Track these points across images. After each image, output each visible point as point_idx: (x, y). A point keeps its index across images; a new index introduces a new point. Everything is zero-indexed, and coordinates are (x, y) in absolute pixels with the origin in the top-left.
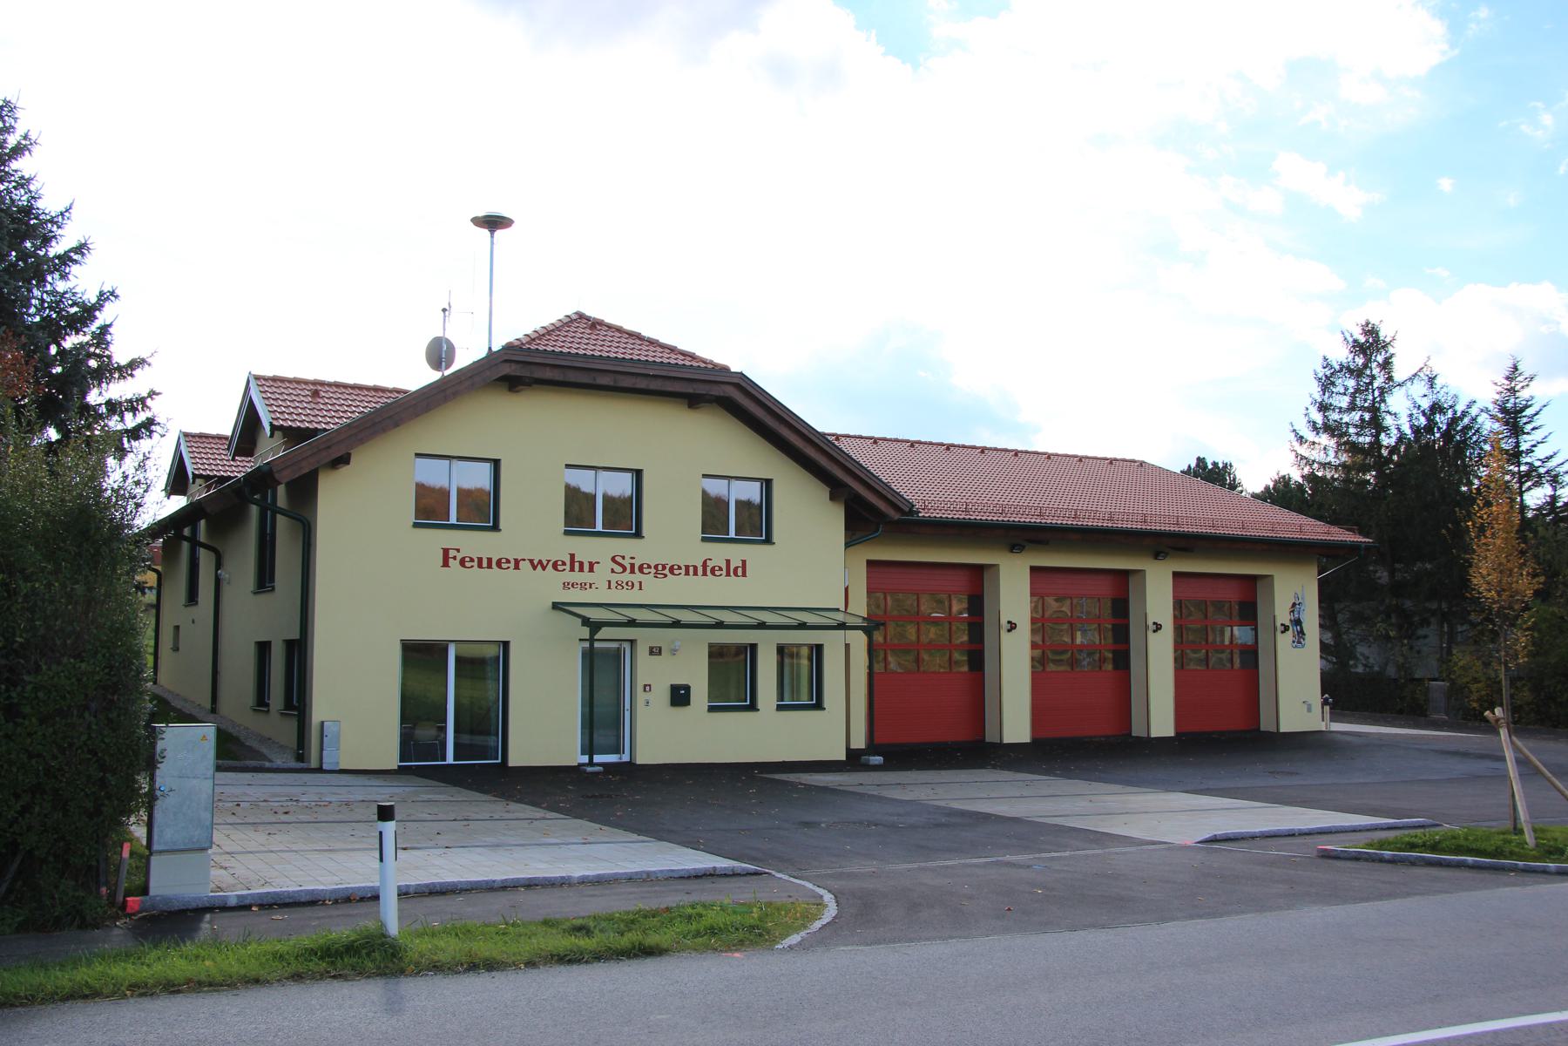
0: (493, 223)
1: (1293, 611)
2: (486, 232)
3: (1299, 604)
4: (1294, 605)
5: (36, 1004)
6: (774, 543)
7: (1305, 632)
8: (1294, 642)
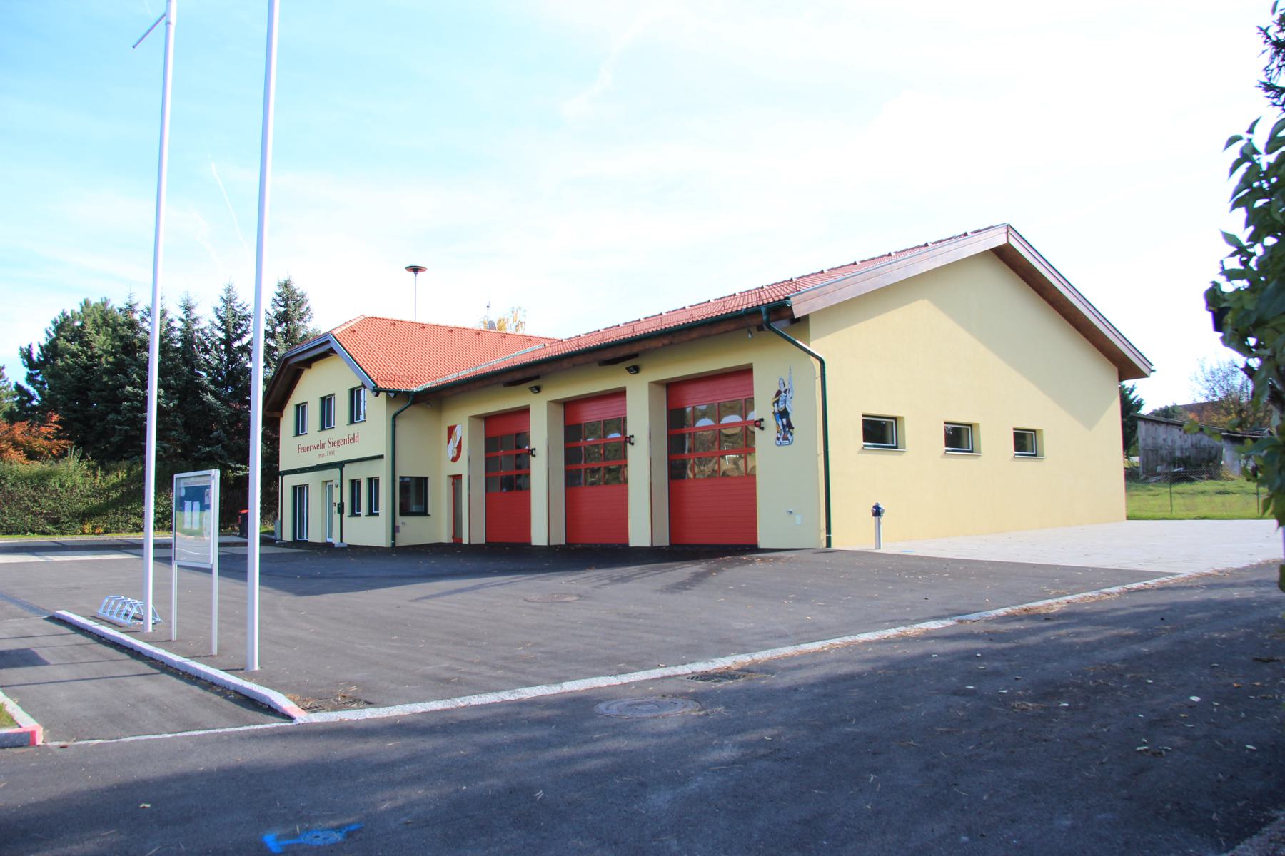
0: (416, 270)
1: (777, 402)
2: (413, 274)
3: (785, 392)
4: (779, 393)
5: (250, 365)
6: (429, 515)
7: (793, 425)
8: (778, 439)
